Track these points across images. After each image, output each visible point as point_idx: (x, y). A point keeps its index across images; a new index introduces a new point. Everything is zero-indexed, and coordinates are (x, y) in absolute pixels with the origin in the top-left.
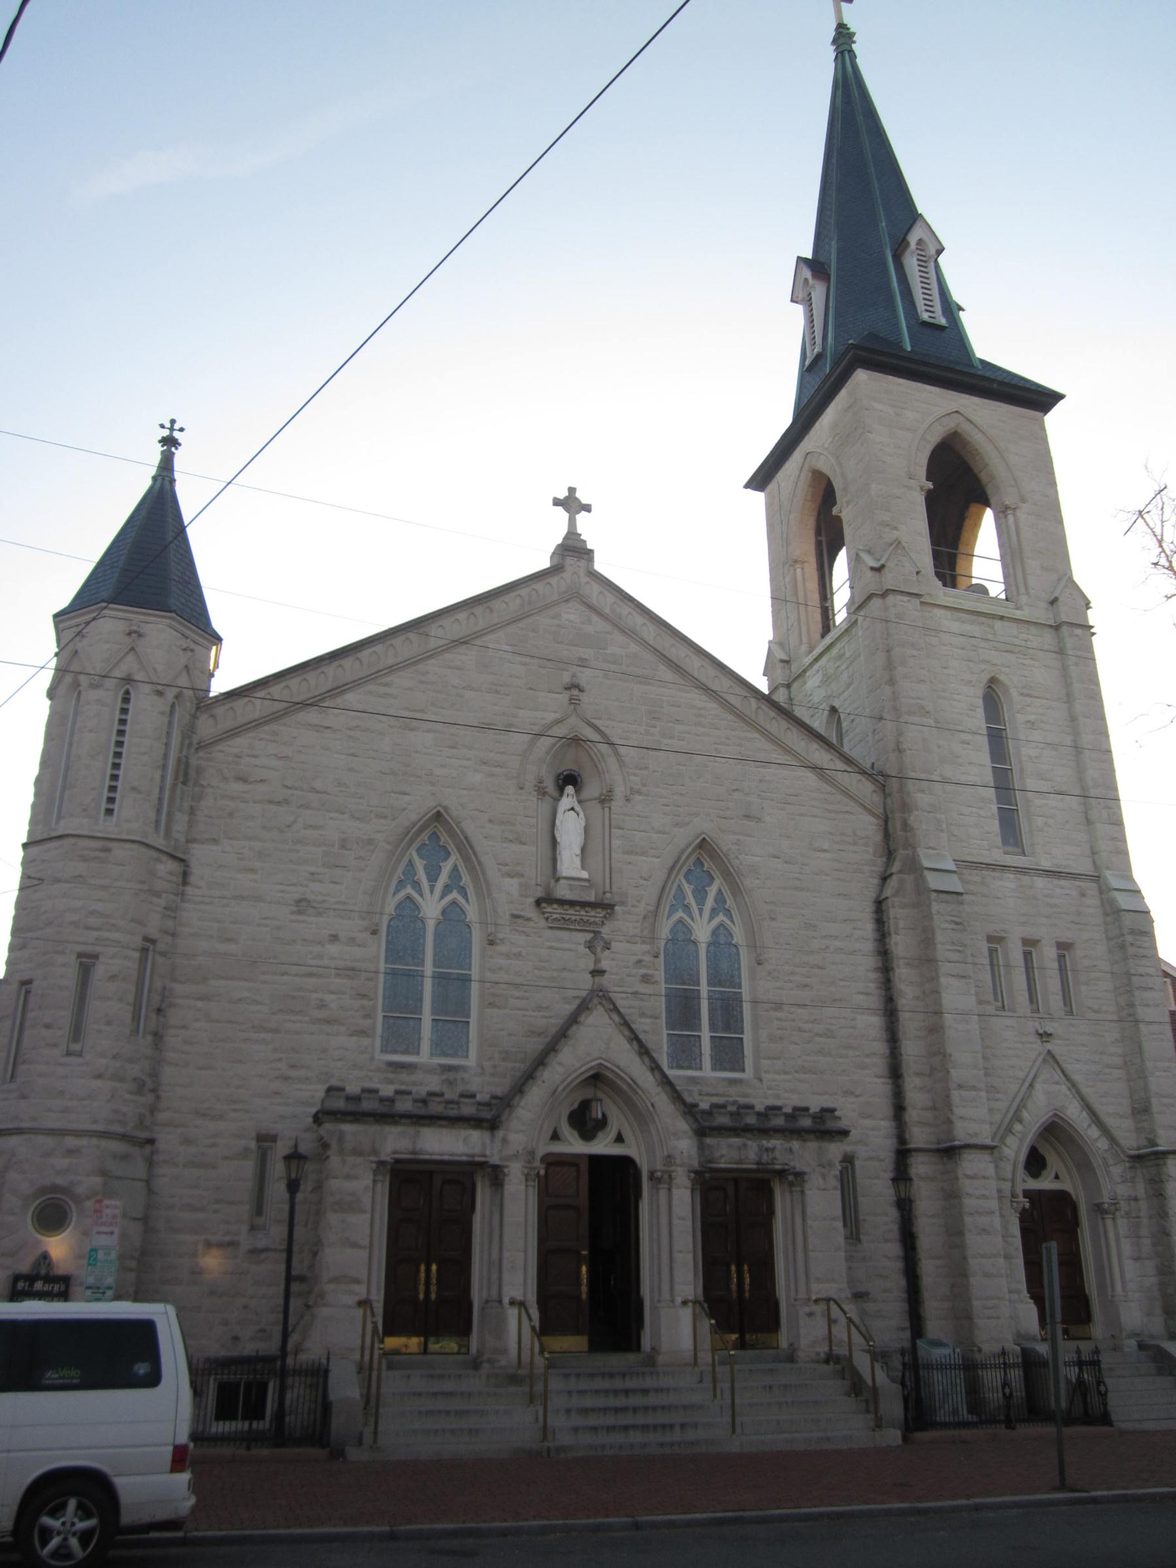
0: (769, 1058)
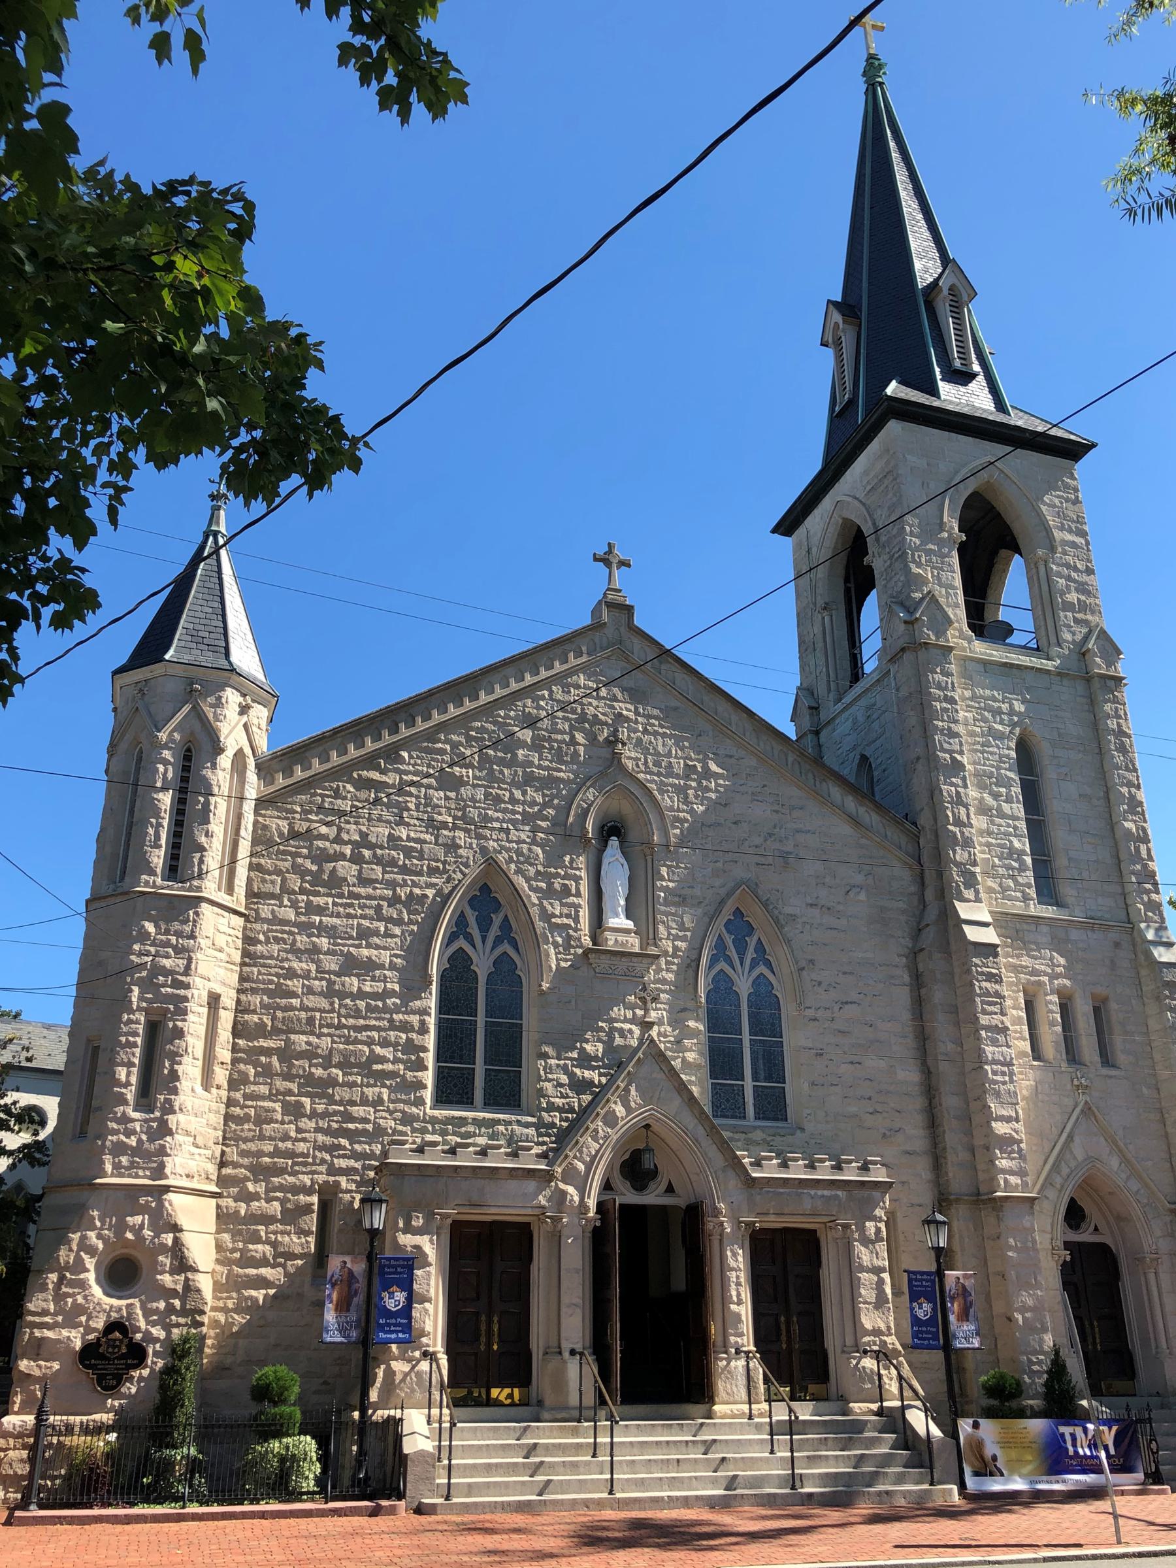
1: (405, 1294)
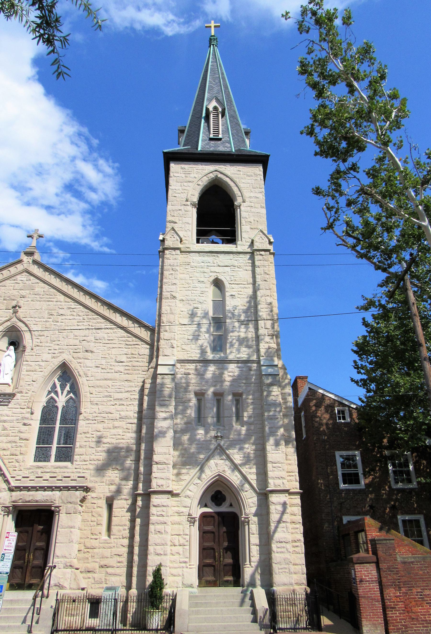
0: (79, 455)
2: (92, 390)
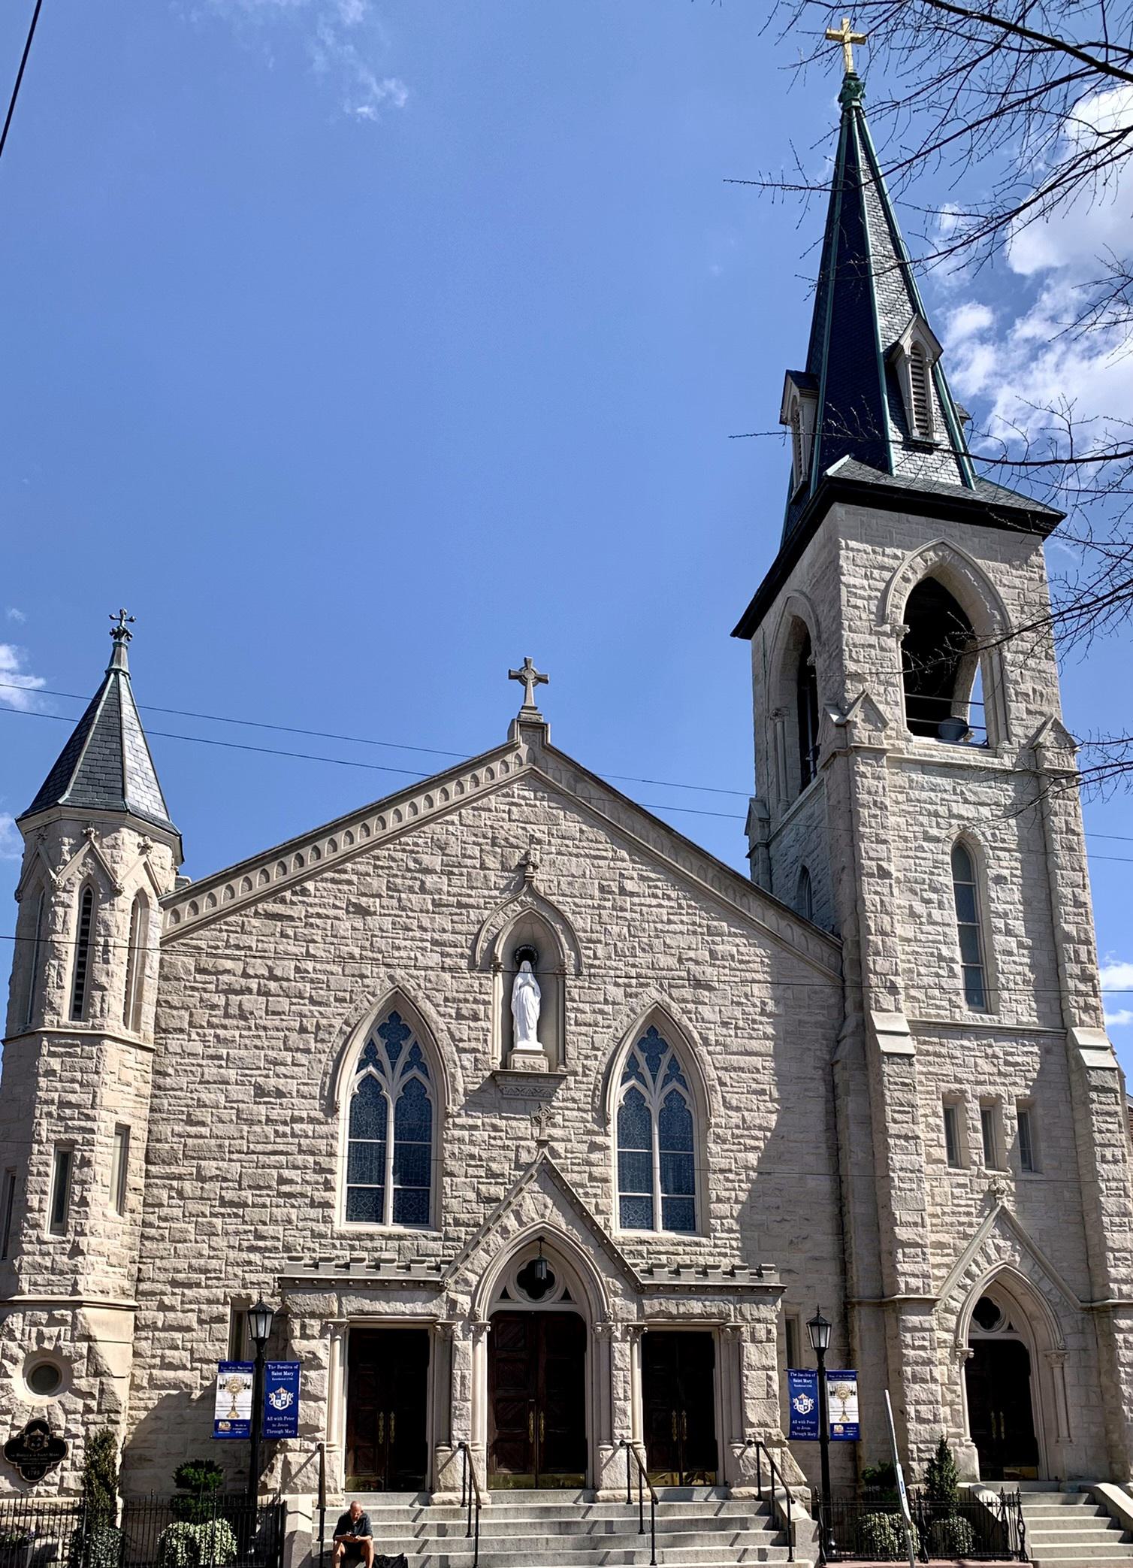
1: (291, 1395)
2: (726, 1077)
